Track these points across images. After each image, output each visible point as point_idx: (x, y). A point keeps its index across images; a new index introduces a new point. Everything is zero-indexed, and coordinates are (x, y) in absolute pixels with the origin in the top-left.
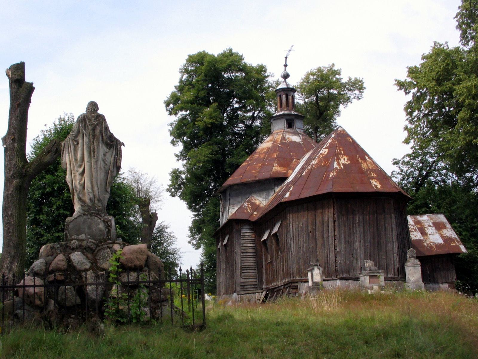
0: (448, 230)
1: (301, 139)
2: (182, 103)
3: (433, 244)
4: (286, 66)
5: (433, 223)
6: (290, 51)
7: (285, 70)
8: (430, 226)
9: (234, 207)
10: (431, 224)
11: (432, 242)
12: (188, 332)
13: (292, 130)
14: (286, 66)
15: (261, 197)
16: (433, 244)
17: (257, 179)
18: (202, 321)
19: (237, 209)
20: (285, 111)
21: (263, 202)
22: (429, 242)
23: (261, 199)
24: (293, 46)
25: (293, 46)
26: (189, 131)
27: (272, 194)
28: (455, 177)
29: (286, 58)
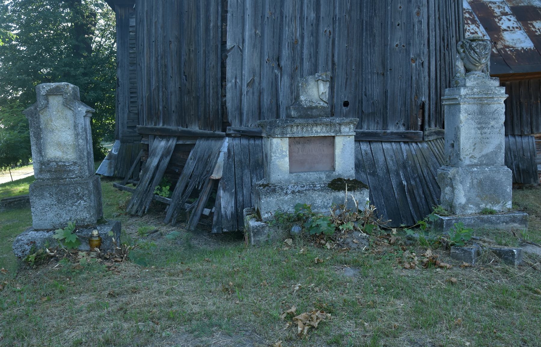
5: (512, 9)
8: (506, 14)
10: (507, 10)
11: (508, 47)
16: (511, 51)
22: (502, 47)
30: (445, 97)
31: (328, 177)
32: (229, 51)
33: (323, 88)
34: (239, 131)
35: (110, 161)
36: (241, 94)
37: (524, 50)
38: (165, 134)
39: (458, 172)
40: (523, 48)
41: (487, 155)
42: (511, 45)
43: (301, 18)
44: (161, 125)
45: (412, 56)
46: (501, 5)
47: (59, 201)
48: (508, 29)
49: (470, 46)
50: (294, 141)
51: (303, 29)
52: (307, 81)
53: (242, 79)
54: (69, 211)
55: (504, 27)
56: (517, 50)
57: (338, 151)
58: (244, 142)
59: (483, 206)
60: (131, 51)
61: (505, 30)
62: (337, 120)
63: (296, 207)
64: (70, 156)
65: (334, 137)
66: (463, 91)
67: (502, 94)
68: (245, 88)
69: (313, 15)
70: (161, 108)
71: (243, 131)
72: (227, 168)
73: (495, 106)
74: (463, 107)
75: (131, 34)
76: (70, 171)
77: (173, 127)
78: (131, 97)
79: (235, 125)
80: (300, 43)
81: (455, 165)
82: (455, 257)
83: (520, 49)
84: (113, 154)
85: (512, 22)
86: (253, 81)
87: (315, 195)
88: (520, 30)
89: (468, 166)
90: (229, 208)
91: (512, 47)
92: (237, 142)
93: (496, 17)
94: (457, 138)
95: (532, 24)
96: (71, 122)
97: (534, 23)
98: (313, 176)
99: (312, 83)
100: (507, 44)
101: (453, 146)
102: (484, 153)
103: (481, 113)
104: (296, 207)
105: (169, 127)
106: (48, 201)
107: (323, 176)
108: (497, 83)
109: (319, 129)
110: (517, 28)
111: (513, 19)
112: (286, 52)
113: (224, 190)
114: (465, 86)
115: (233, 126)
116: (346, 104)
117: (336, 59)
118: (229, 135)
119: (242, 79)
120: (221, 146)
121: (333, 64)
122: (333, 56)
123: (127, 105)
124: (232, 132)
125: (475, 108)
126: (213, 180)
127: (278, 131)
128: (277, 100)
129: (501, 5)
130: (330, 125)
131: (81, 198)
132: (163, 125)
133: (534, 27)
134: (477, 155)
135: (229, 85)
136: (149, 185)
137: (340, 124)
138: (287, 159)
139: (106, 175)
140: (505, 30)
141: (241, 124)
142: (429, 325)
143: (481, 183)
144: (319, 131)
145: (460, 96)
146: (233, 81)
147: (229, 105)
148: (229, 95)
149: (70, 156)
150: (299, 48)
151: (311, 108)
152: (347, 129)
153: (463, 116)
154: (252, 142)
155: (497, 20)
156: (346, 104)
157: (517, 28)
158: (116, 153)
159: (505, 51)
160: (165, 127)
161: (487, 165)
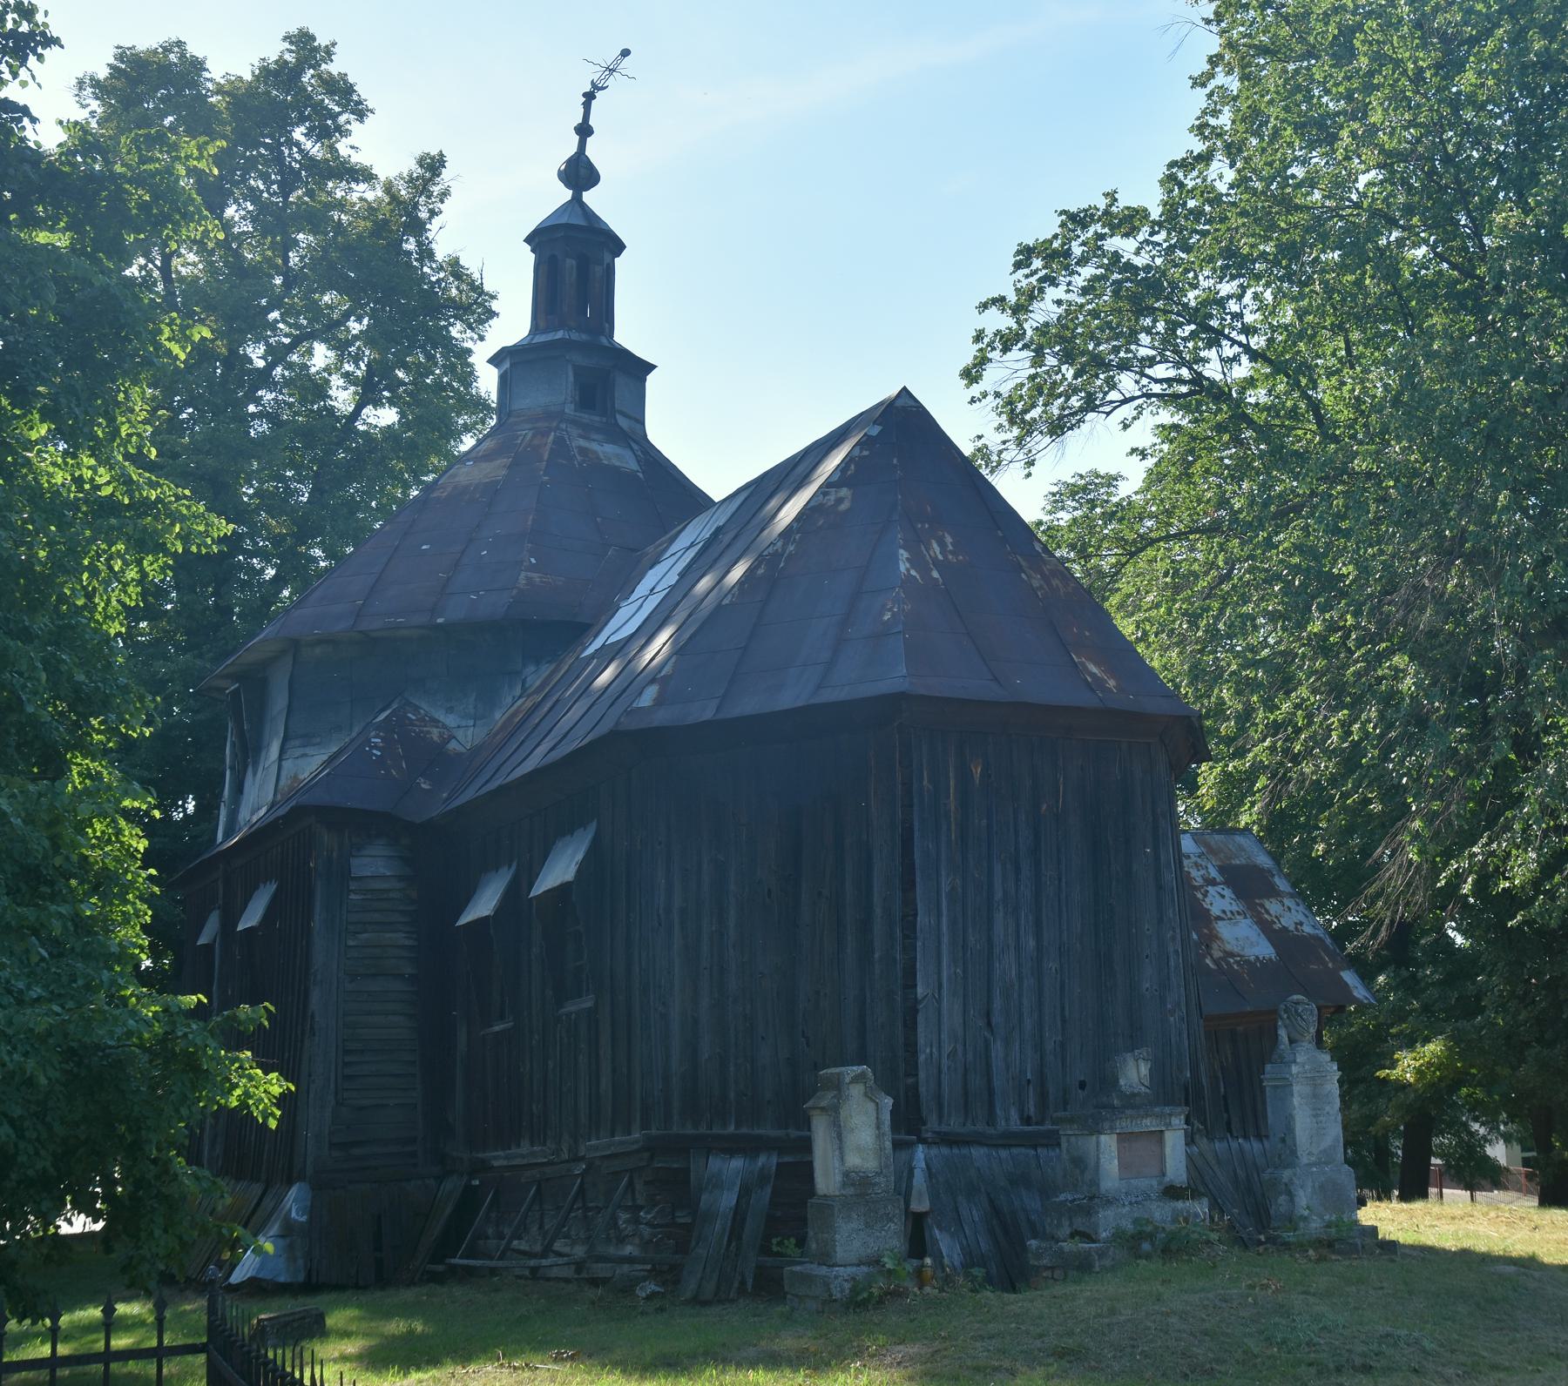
0: (1287, 902)
1: (638, 462)
2: (1389, 668)
3: (1237, 963)
4: (584, 130)
5: (1222, 870)
6: (612, 71)
7: (582, 145)
8: (1213, 882)
9: (308, 750)
10: (1214, 873)
11: (1232, 955)
12: (661, 1310)
13: (597, 418)
14: (584, 130)
15: (450, 710)
16: (1237, 963)
17: (440, 620)
18: (168, 1314)
19: (325, 757)
20: (570, 329)
21: (460, 734)
22: (1221, 954)
23: (450, 720)
24: (625, 53)
25: (625, 53)
26: (1324, 712)
27: (509, 700)
28: (1304, 688)
29: (589, 97)
30: (1268, 1076)
31: (1160, 1183)
32: (921, 1001)
33: (1144, 1069)
34: (938, 1133)
35: (288, 1240)
36: (940, 1072)
37: (1261, 962)
38: (732, 1147)
39: (1295, 1174)
40: (1257, 958)
41: (1325, 1150)
42: (1236, 950)
43: (1018, 948)
44: (731, 1129)
45: (1169, 1006)
46: (1199, 861)
47: (867, 1225)
48: (1223, 915)
49: (1296, 1011)
50: (1124, 1138)
51: (1020, 965)
52: (1125, 1060)
53: (940, 1047)
54: (878, 1238)
55: (1215, 911)
56: (1248, 962)
57: (1168, 1150)
58: (945, 1151)
59: (1327, 1217)
60: (351, 943)
61: (1219, 918)
62: (1167, 1110)
63: (1136, 1221)
64: (871, 1164)
65: (1162, 1131)
66: (1295, 1069)
67: (1333, 1072)
68: (945, 1061)
69: (1032, 943)
70: (732, 1095)
71: (945, 1133)
72: (934, 1196)
73: (1328, 1087)
74: (1296, 1088)
75: (352, 896)
76: (875, 1184)
77: (768, 1131)
78: (346, 1064)
79: (932, 1124)
80: (1016, 987)
81: (1291, 1165)
82: (1339, 1252)
83: (1252, 958)
84: (296, 1221)
85: (1228, 900)
86: (955, 1049)
87: (1154, 1206)
88: (1245, 918)
89: (1308, 1165)
90: (956, 1256)
91: (1239, 956)
92: (934, 1151)
93: (1197, 888)
94: (1290, 1129)
95: (1262, 906)
96: (873, 1118)
97: (1267, 904)
98: (1143, 1183)
99: (1131, 1063)
100: (1228, 948)
101: (1283, 1140)
102: (1322, 1148)
103: (1315, 1096)
104: (1136, 1221)
105: (761, 1132)
106: (854, 1225)
107: (1154, 1183)
108: (1327, 1057)
109: (1147, 1121)
110: (1238, 913)
111: (1228, 892)
112: (998, 1004)
113: (940, 1230)
114: (1295, 1062)
115: (929, 1125)
116: (1082, 1085)
117: (1067, 1013)
118: (923, 1141)
119: (940, 1047)
120: (911, 1159)
121: (1064, 1021)
122: (1063, 1009)
123: (332, 1086)
124: (929, 1135)
125: (1307, 1090)
126: (914, 1213)
127: (1106, 1125)
128: (989, 1081)
129: (1199, 861)
130: (1160, 1116)
131: (891, 1220)
132: (736, 1129)
133: (1268, 912)
134: (1315, 1151)
135: (922, 1058)
136: (729, 1242)
137: (1170, 1115)
138: (1116, 1161)
139: (282, 1279)
140: (1219, 918)
141: (940, 1123)
142: (1322, 1329)
143: (1322, 1187)
144: (1149, 1124)
145: (1291, 1075)
146: (928, 1051)
147: (922, 1090)
148: (922, 1075)
149: (871, 1164)
150: (1016, 996)
151: (1134, 1095)
152: (1177, 1122)
153: (1296, 1101)
154: (956, 1151)
155: (1199, 896)
156: (1082, 1085)
157: (1238, 913)
158: (304, 1219)
159: (1228, 963)
160: (744, 1130)
161: (1326, 1163)
